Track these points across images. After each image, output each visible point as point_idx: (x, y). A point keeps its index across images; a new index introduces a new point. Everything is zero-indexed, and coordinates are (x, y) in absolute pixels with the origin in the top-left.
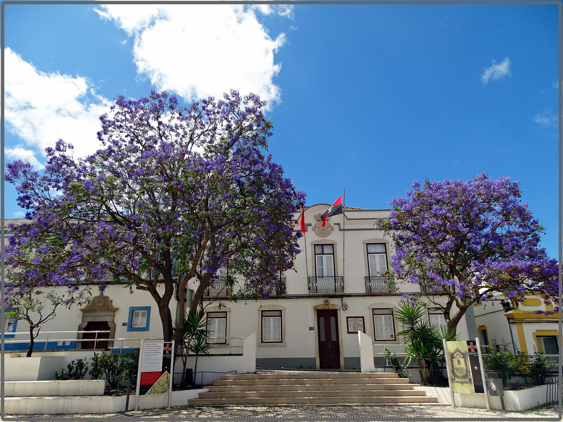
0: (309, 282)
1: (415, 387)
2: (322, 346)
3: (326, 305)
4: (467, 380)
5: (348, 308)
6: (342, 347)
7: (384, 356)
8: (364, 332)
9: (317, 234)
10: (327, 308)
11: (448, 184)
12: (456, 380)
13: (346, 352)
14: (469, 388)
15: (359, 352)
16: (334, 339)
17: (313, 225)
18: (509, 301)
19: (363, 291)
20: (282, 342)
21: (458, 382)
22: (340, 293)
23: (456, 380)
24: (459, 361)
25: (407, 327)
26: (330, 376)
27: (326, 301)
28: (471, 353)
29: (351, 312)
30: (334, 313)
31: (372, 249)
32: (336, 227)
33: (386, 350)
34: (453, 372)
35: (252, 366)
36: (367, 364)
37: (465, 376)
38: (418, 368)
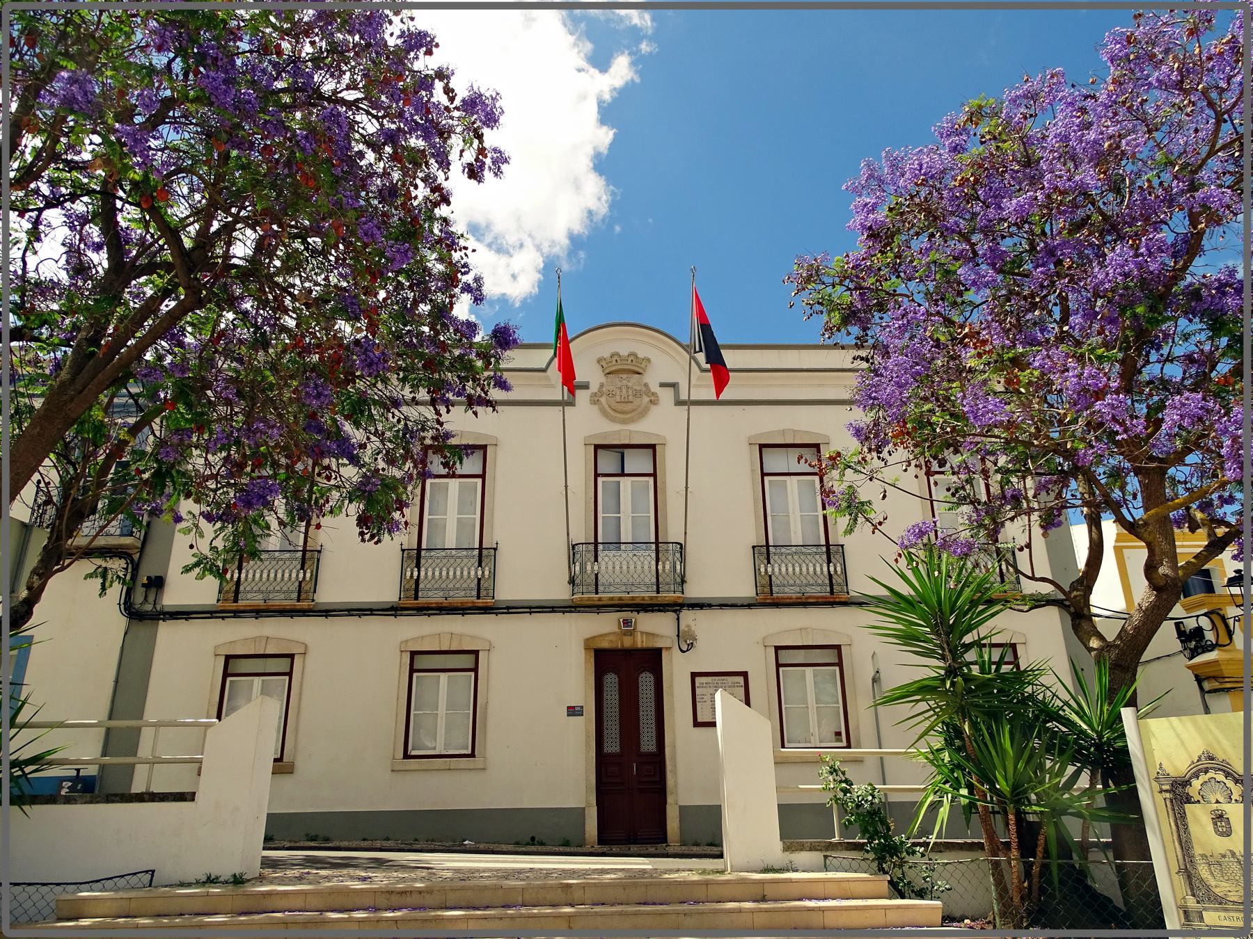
0: (572, 561)
2: (610, 773)
3: (625, 633)
5: (698, 645)
6: (675, 773)
7: (826, 799)
8: (748, 703)
9: (604, 413)
10: (628, 643)
13: (684, 790)
15: (717, 788)
16: (648, 744)
17: (594, 388)
18: (1205, 623)
19: (746, 590)
20: (472, 755)
22: (668, 596)
25: (929, 668)
26: (578, 895)
27: (627, 622)
29: (702, 660)
30: (652, 659)
31: (776, 461)
32: (666, 396)
33: (833, 771)
34: (1188, 873)
35: (241, 846)
36: (751, 834)
38: (980, 846)
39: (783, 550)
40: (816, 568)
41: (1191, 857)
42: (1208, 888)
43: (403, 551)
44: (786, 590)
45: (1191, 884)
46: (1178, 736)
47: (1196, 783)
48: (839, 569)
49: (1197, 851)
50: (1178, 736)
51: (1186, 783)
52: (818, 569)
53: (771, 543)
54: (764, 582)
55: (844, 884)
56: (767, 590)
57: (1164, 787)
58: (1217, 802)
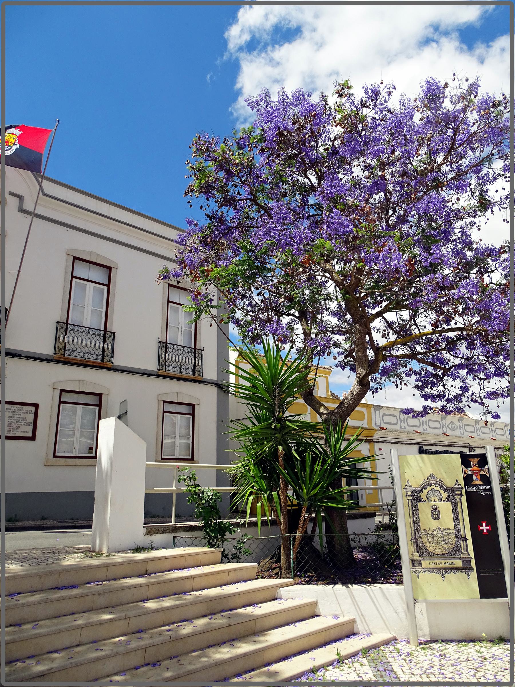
1: (283, 592)
4: (459, 563)
11: (439, 82)
12: (425, 564)
14: (466, 585)
19: (48, 350)
21: (430, 570)
23: (425, 564)
24: (435, 510)
28: (472, 489)
31: (81, 271)
34: (416, 540)
37: (455, 552)
39: (77, 328)
40: (96, 343)
41: (419, 531)
42: (425, 547)
43: (160, 342)
44: (75, 354)
45: (417, 546)
46: (419, 465)
47: (425, 491)
48: (110, 347)
49: (422, 528)
50: (419, 465)
51: (421, 491)
52: (97, 345)
53: (69, 322)
54: (61, 346)
55: (197, 557)
56: (62, 352)
57: (409, 493)
58: (435, 501)
